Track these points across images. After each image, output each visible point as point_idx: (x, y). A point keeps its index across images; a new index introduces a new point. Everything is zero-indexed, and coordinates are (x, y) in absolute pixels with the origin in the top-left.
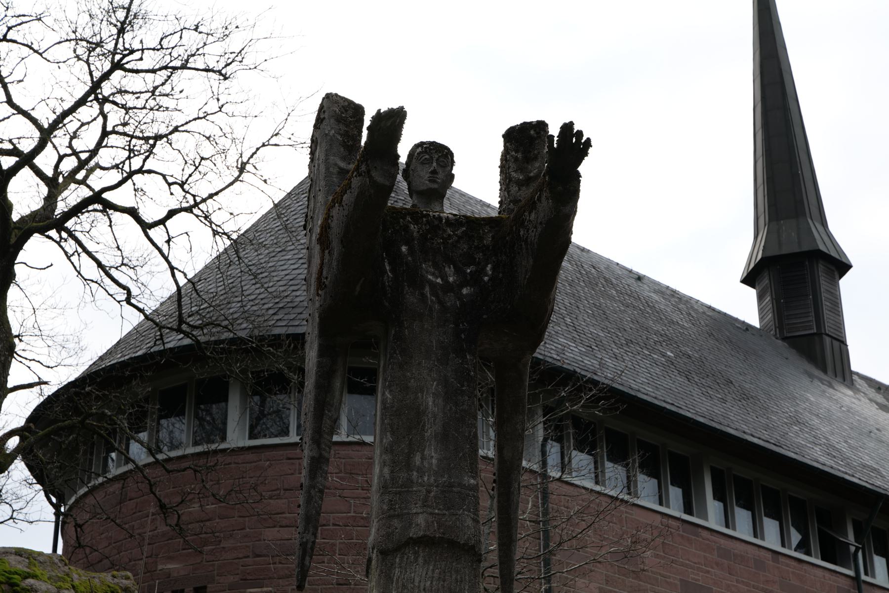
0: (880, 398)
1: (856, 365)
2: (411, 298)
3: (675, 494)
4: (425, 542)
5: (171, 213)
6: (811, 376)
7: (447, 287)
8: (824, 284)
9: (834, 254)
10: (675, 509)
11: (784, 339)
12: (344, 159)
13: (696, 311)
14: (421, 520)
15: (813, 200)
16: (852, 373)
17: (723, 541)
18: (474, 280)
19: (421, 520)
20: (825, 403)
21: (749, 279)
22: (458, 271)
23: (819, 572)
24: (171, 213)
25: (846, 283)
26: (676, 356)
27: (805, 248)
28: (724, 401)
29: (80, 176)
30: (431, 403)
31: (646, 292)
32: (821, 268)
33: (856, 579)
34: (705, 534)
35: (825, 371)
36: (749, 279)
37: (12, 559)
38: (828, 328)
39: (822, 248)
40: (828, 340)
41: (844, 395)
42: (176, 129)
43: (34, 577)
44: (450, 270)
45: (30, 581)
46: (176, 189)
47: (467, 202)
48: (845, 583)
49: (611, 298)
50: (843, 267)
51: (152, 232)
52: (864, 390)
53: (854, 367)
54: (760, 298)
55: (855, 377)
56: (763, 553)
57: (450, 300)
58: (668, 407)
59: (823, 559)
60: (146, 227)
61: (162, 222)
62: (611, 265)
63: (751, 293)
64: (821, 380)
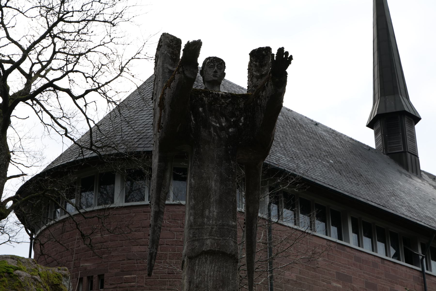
1: (423, 167)
2: (204, 133)
3: (334, 230)
4: (211, 253)
5: (87, 92)
6: (401, 173)
7: (222, 128)
8: (407, 127)
9: (412, 112)
10: (334, 237)
11: (388, 154)
12: (171, 65)
13: (344, 140)
14: (208, 242)
15: (402, 86)
16: (421, 171)
17: (357, 254)
18: (235, 125)
19: (208, 242)
20: (407, 186)
21: (370, 125)
22: (227, 120)
23: (404, 269)
24: (87, 92)
25: (418, 127)
26: (335, 162)
27: (398, 110)
28: (358, 185)
29: (42, 73)
30: (213, 185)
31: (320, 131)
32: (406, 120)
33: (422, 272)
34: (348, 249)
35: (407, 170)
36: (370, 125)
37: (9, 261)
38: (409, 149)
39: (406, 109)
40: (409, 155)
41: (417, 182)
42: (89, 51)
43: (20, 269)
44: (223, 120)
45: (18, 271)
46: (89, 80)
47: (232, 86)
48: (417, 274)
49: (303, 134)
50: (417, 119)
51: (77, 101)
52: (427, 179)
53: (422, 169)
54: (376, 134)
55: (422, 173)
56: (377, 259)
57: (223, 135)
58: (331, 187)
59: (406, 262)
60: (74, 98)
61: (83, 96)
62: (302, 118)
63: (371, 132)
64: (406, 175)
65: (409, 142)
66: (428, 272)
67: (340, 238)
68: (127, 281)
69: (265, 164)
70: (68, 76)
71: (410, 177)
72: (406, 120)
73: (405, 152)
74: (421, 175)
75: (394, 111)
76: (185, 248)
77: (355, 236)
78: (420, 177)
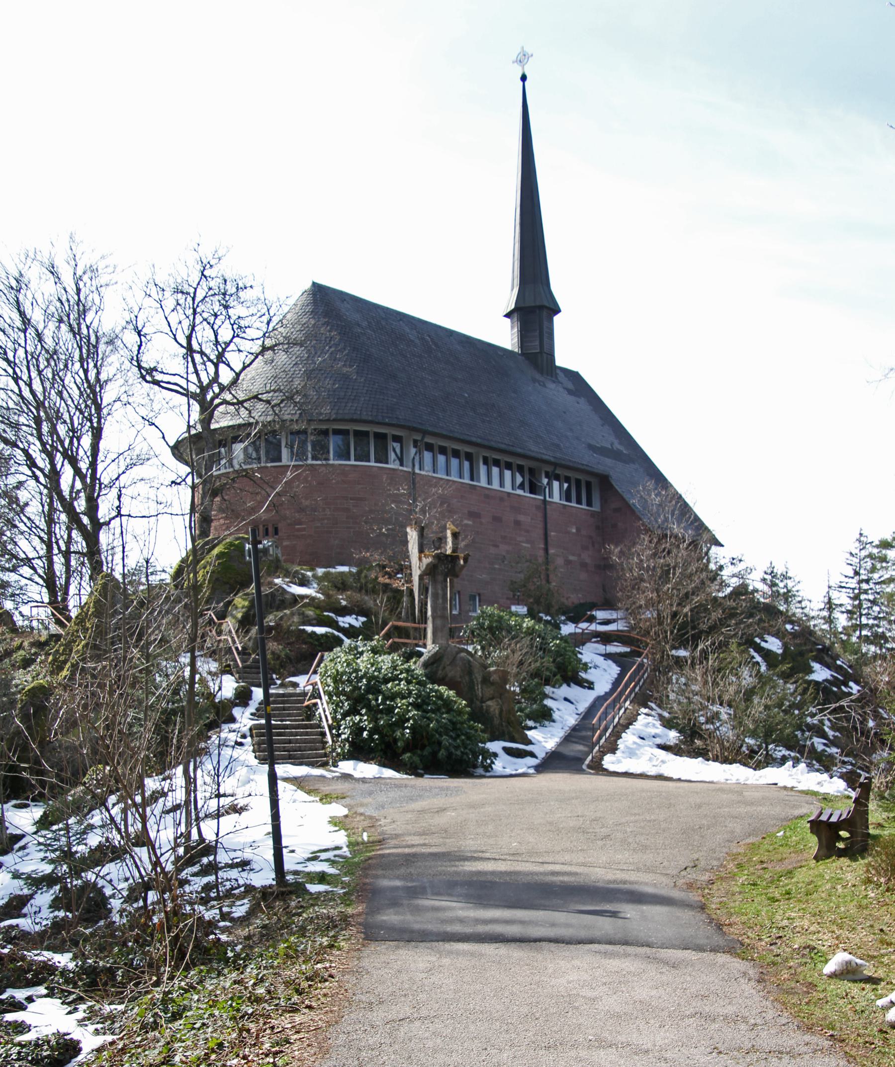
0: (570, 386)
6: (534, 380)
8: (545, 323)
25: (556, 319)
27: (538, 304)
33: (545, 501)
35: (542, 373)
39: (546, 304)
40: (545, 355)
50: (557, 311)
54: (512, 323)
55: (558, 371)
64: (539, 382)
65: (546, 340)
66: (550, 500)
67: (472, 479)
68: (299, 530)
69: (409, 571)
70: (232, 369)
71: (544, 386)
72: (545, 313)
73: (541, 352)
74: (556, 374)
75: (533, 304)
76: (400, 918)
77: (485, 467)
78: (556, 381)
